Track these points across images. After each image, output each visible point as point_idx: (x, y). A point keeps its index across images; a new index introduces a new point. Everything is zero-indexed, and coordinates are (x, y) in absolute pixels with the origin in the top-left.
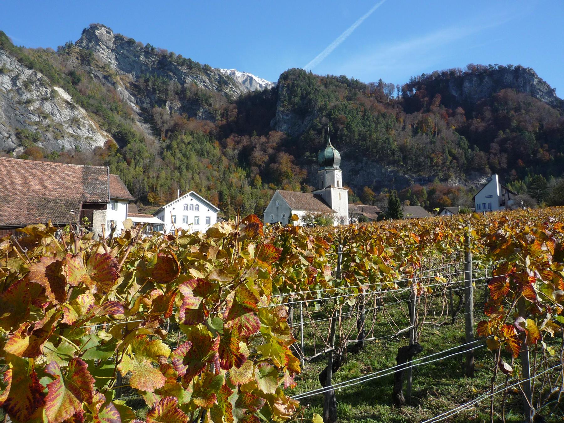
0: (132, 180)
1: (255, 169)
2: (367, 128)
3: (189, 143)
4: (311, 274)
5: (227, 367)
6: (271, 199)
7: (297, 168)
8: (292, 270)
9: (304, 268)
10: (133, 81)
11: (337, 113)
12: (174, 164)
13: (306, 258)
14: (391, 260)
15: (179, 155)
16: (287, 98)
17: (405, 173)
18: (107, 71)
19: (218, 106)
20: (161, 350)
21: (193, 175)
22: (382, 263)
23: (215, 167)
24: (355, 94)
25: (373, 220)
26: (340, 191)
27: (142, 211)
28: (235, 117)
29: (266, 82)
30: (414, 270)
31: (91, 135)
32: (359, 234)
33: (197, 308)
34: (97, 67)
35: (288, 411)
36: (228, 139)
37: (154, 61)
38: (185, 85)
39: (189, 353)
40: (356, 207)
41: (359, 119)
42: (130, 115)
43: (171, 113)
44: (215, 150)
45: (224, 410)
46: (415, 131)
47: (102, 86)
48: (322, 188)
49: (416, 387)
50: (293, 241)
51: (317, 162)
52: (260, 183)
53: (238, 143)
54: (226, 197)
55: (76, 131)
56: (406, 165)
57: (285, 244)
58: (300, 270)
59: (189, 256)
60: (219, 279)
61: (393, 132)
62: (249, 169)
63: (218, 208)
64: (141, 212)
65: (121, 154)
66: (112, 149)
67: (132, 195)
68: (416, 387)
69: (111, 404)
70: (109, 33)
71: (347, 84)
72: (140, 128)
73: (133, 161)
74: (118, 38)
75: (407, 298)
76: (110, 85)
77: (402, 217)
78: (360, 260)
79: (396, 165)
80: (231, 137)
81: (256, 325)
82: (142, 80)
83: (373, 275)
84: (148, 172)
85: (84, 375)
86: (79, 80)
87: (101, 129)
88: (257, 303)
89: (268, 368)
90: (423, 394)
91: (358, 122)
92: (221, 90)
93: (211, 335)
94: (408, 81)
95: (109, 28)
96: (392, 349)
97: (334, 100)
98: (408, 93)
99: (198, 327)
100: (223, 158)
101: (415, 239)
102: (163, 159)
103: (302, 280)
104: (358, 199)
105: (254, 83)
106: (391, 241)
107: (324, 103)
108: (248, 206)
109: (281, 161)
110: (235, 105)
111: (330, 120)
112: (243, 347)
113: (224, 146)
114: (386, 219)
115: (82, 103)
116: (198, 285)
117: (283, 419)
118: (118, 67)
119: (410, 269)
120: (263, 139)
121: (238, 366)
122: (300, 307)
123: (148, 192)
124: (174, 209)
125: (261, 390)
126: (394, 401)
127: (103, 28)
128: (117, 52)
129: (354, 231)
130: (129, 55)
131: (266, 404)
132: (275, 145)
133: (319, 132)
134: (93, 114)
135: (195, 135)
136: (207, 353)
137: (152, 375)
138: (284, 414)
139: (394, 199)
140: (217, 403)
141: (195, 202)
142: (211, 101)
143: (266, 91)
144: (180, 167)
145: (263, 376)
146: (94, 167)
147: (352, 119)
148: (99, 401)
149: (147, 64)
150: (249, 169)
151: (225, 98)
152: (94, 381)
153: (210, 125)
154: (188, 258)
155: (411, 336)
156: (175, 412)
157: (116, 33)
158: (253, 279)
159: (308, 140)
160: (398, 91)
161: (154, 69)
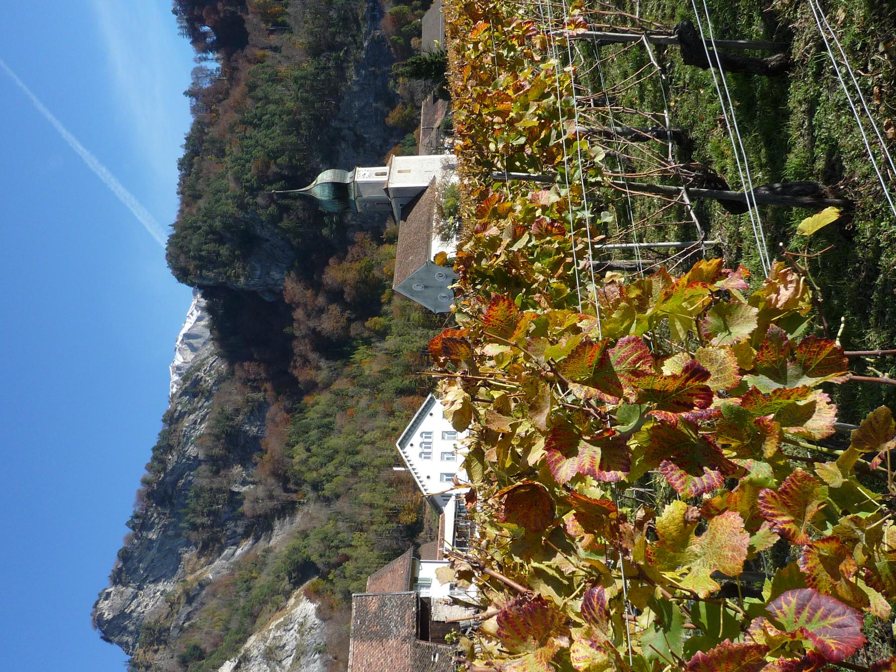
0: (376, 553)
1: (355, 329)
2: (276, 119)
3: (308, 450)
4: (546, 229)
5: (707, 395)
6: (410, 300)
7: (353, 251)
8: (537, 265)
9: (534, 242)
10: (195, 551)
11: (248, 176)
12: (347, 476)
13: (515, 238)
14: (521, 76)
15: (330, 468)
16: (221, 270)
17: (360, 47)
18: (179, 598)
19: (239, 398)
20: (674, 519)
21: (366, 443)
22: (526, 94)
23: (350, 402)
24: (213, 142)
25: (449, 109)
26: (394, 172)
27: (433, 534)
28: (259, 366)
29: (192, 308)
30: (538, 33)
31: (296, 626)
32: (471, 137)
33: (598, 450)
34: (172, 616)
35: (791, 282)
36: (300, 379)
37: (159, 514)
38: (201, 457)
39: (681, 466)
40: (423, 140)
41: (260, 135)
42: (257, 557)
43: (253, 483)
44: (319, 403)
45: (785, 402)
46: (282, 27)
47: (206, 607)
48: (390, 204)
49: (757, 31)
50: (483, 262)
51: (342, 214)
52: (381, 319)
53: (306, 361)
54: (407, 382)
55: (289, 653)
56: (346, 45)
57: (489, 276)
58: (538, 250)
59: (503, 463)
60: (547, 411)
61: (283, 69)
62: (355, 339)
63: (426, 396)
64: (435, 535)
65: (329, 573)
66: (321, 587)
67: (403, 552)
68: (757, 31)
69: (768, 609)
70: (109, 594)
71: (193, 158)
72: (281, 538)
73: (342, 551)
74: (118, 578)
75: (593, 47)
76: (204, 592)
77: (443, 53)
78: (521, 136)
79: (345, 65)
80: (295, 373)
81: (632, 344)
82: (194, 535)
83: (549, 112)
84: (362, 523)
85: (716, 659)
86: (196, 648)
87: (284, 607)
88: (591, 343)
89: (712, 320)
90: (770, 19)
91: (266, 136)
92: (210, 392)
93: (649, 426)
94: (187, 41)
95: (100, 595)
96: (687, 76)
97: (225, 181)
98: (209, 40)
99: (633, 447)
100: (334, 387)
101: (481, 32)
102: (338, 496)
103: (556, 246)
104: (409, 137)
105: (195, 331)
106: (485, 77)
107: (230, 201)
108: (424, 343)
109: (339, 281)
110: (237, 366)
111: (260, 188)
112: (671, 367)
113: (312, 387)
114: (446, 83)
115: (237, 643)
116: (559, 448)
117: (805, 291)
118: (170, 578)
119: (537, 41)
120: (299, 314)
121: (706, 375)
122: (608, 249)
123: (399, 523)
124: (428, 477)
125: (750, 334)
126: (782, 74)
127: (101, 605)
128: (144, 581)
129: (466, 147)
130: (149, 558)
131: (777, 323)
132: (309, 293)
133: (285, 210)
134: (258, 622)
135: (294, 438)
136: (684, 434)
137: (718, 536)
138: (797, 289)
139: (408, 69)
140: (772, 416)
141: (416, 439)
142: (229, 409)
143: (209, 309)
144: (352, 467)
145: (726, 328)
146: (353, 621)
147: (259, 148)
148: (764, 630)
149: (164, 526)
150: (355, 339)
151: (223, 385)
152: (727, 641)
153: (275, 411)
154: (508, 465)
155: (662, 41)
156: (787, 493)
157: (107, 582)
158: (548, 346)
159: (301, 230)
160: (206, 59)
161: (174, 514)
